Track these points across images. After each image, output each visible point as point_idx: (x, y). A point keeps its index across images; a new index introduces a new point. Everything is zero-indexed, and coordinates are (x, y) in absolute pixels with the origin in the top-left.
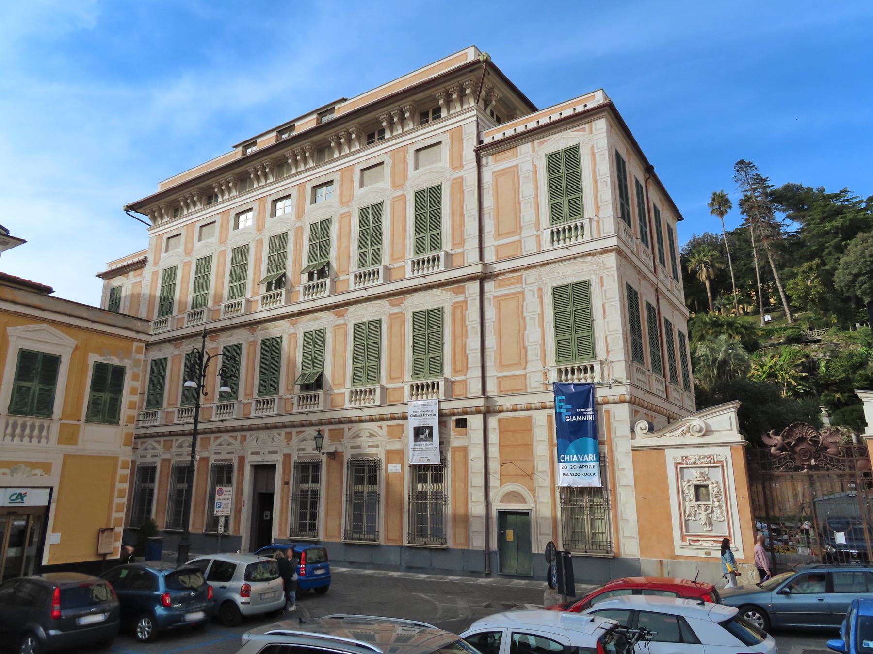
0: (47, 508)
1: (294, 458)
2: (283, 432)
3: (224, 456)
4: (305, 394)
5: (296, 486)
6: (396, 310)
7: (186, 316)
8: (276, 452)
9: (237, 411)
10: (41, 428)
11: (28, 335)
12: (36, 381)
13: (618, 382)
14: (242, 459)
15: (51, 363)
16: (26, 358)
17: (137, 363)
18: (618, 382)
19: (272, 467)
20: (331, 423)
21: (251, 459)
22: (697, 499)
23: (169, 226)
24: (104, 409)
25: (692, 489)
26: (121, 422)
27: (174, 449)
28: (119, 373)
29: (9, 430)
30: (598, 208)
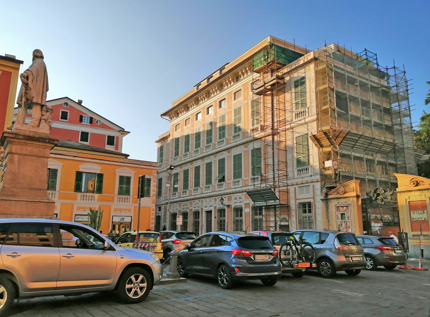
0: (131, 222)
2: (214, 198)
3: (197, 208)
4: (219, 183)
6: (246, 149)
8: (212, 206)
9: (199, 191)
10: (127, 199)
11: (121, 171)
12: (125, 185)
14: (202, 209)
15: (129, 179)
16: (121, 178)
17: (154, 177)
18: (316, 174)
19: (211, 212)
22: (342, 219)
23: (176, 121)
25: (340, 214)
26: (131, 195)
27: (182, 207)
29: (119, 199)
30: (311, 103)
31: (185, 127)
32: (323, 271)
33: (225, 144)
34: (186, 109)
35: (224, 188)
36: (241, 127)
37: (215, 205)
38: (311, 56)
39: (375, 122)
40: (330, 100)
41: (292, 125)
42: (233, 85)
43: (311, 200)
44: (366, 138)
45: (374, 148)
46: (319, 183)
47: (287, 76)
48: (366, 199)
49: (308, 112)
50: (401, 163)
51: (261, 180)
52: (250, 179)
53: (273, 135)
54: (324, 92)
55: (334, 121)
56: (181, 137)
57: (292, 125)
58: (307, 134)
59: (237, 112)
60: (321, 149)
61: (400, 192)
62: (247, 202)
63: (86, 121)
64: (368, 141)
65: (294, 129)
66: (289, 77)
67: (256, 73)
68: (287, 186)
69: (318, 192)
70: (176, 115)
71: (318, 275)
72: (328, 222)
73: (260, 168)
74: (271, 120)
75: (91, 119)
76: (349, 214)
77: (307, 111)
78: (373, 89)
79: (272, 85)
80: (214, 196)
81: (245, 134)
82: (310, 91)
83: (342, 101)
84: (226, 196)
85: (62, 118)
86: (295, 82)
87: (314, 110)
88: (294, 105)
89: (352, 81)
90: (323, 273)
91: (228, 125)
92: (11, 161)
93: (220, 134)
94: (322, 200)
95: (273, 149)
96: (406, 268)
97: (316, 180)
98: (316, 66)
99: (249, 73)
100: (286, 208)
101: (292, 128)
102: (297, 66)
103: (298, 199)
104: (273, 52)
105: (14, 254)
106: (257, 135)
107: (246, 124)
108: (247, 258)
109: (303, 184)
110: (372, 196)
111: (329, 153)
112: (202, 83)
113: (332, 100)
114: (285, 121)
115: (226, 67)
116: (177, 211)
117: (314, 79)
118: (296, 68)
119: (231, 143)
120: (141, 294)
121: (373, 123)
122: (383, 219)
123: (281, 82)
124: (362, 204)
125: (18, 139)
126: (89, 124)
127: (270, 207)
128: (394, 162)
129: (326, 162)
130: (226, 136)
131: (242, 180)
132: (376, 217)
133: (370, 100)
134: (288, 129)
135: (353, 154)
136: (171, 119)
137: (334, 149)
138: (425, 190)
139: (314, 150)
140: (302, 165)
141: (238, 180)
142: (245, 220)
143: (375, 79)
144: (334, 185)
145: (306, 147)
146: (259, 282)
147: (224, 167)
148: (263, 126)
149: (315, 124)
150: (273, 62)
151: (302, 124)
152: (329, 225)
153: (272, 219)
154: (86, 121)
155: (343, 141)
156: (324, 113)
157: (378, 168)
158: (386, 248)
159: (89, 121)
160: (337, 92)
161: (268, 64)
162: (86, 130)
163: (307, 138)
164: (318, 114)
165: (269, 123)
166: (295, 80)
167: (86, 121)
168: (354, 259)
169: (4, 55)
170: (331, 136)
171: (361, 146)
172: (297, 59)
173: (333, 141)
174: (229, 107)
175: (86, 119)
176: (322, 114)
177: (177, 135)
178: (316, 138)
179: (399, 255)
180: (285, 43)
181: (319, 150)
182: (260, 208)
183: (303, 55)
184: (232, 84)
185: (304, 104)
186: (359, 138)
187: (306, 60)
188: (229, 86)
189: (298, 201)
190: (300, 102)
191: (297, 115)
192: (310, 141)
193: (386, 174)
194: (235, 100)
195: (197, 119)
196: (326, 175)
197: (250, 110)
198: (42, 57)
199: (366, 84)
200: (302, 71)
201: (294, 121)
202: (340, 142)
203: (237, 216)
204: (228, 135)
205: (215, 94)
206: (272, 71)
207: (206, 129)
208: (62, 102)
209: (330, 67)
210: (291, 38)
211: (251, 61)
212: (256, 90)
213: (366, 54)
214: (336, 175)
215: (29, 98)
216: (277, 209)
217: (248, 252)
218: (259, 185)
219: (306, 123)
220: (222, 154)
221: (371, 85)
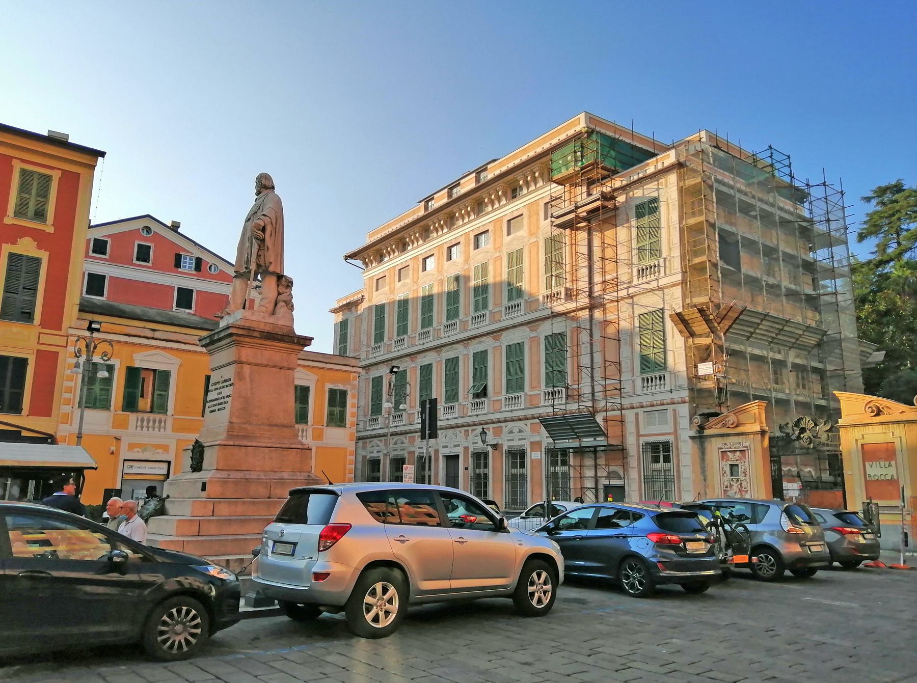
1: (471, 450)
2: (462, 429)
4: (475, 401)
5: (473, 471)
6: (534, 334)
7: (393, 342)
8: (458, 446)
10: (160, 422)
13: (680, 388)
14: (437, 451)
18: (680, 388)
19: (457, 457)
20: (493, 423)
21: (444, 452)
22: (732, 474)
23: (377, 270)
24: (337, 419)
25: (728, 467)
26: (168, 413)
27: (391, 446)
28: (344, 394)
29: (139, 423)
30: (670, 249)
31: (398, 284)
32: (760, 569)
33: (487, 322)
34: (401, 246)
35: (486, 411)
36: (523, 288)
37: (466, 445)
38: (670, 158)
39: (788, 289)
40: (709, 246)
41: (631, 290)
42: (505, 205)
43: (671, 438)
44: (775, 320)
45: (789, 339)
46: (687, 405)
47: (621, 194)
48: (778, 437)
49: (665, 267)
50: (835, 368)
51: (567, 398)
52: (542, 394)
53: (591, 308)
54: (696, 229)
55: (715, 287)
56: (389, 303)
57: (631, 290)
58: (662, 309)
59: (515, 258)
60: (690, 340)
61: (845, 427)
62: (536, 438)
63: (188, 265)
64: (777, 326)
65: (635, 299)
66: (624, 196)
67: (555, 185)
68: (622, 409)
69: (684, 423)
70: (378, 257)
71: (754, 577)
72: (705, 480)
73: (563, 372)
74: (587, 279)
75: (199, 261)
76: (747, 465)
77: (662, 264)
78: (784, 223)
79: (590, 212)
80: (463, 426)
81: (532, 302)
82: (669, 227)
83: (729, 246)
84: (491, 426)
85: (138, 259)
86: (638, 207)
87: (676, 264)
88: (635, 252)
89: (746, 209)
90: (760, 573)
91: (495, 284)
92: (240, 376)
93: (476, 302)
94: (692, 438)
95: (591, 336)
96: (878, 566)
97: (680, 400)
98: (680, 178)
99: (540, 184)
100: (618, 451)
101: (631, 297)
102: (641, 175)
103: (643, 436)
104: (594, 146)
105: (461, 540)
106: (561, 306)
107: (535, 283)
108: (673, 546)
109: (653, 406)
110: (791, 432)
111: (708, 347)
112: (435, 196)
113: (712, 246)
114: (616, 282)
115: (489, 166)
116: (381, 454)
117: (677, 203)
118: (640, 180)
119: (500, 321)
120: (546, 601)
121: (783, 290)
122: (802, 474)
123: (610, 204)
124: (771, 446)
125: (251, 337)
126: (195, 272)
127: (587, 449)
128: (820, 366)
129: (700, 366)
130: (491, 306)
131: (526, 394)
132: (790, 470)
133: (778, 245)
134: (623, 298)
135: (749, 350)
136: (367, 266)
137: (715, 341)
138: (893, 423)
139: (676, 341)
140: (652, 367)
141: (516, 395)
142: (532, 476)
143: (788, 205)
144: (717, 410)
145: (661, 334)
146: (679, 588)
147: (486, 367)
148: (570, 289)
149: (678, 291)
150: (595, 164)
151: (652, 290)
152: (706, 487)
153: (589, 473)
154: (187, 265)
155: (734, 326)
156: (695, 269)
157: (790, 378)
158: (849, 530)
159: (193, 266)
160: (721, 230)
161: (582, 169)
162: (187, 284)
163: (663, 318)
164: (684, 273)
165: (583, 284)
166: (638, 202)
167: (188, 265)
168: (814, 549)
169: (46, 134)
170: (711, 317)
171: (765, 335)
172: (642, 162)
173: (716, 324)
174: (498, 249)
175: (188, 261)
176: (692, 273)
177: (379, 298)
178: (681, 319)
179: (869, 542)
180: (615, 129)
181: (686, 342)
182: (564, 452)
183: (657, 155)
184: (504, 202)
185: (655, 251)
186: (762, 320)
187: (660, 167)
188: (497, 205)
189: (642, 440)
190: (648, 247)
191: (642, 272)
192: (669, 324)
193: (804, 387)
194: (509, 234)
195: (424, 269)
196: (701, 391)
197: (542, 257)
198: (273, 188)
199: (771, 214)
200: (652, 185)
201: (635, 282)
202: (727, 327)
203: (514, 466)
204: (495, 305)
205: (466, 220)
206: (591, 183)
207: (445, 289)
208: (139, 225)
209: (709, 182)
210: (633, 120)
211: (548, 157)
212: (557, 218)
213: (771, 157)
214: (720, 390)
215: (262, 263)
216: (600, 454)
217: (674, 538)
218: (562, 406)
219: (660, 288)
220: (481, 342)
221: (780, 217)
